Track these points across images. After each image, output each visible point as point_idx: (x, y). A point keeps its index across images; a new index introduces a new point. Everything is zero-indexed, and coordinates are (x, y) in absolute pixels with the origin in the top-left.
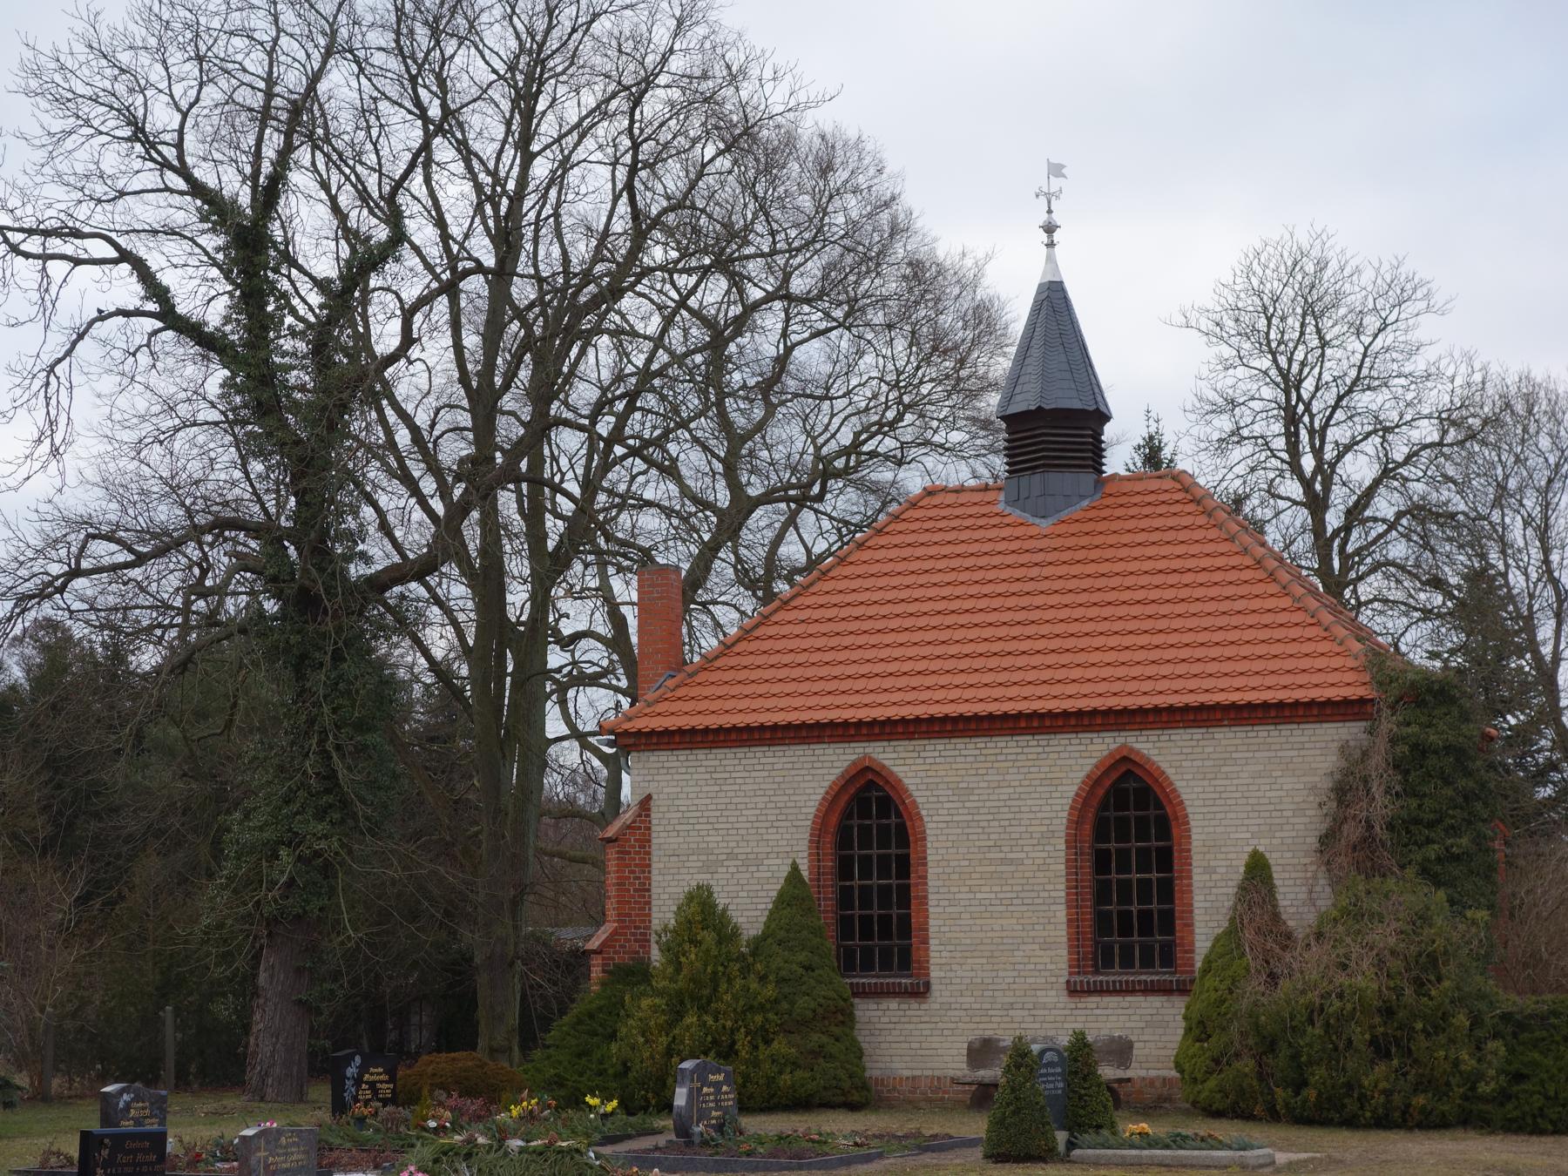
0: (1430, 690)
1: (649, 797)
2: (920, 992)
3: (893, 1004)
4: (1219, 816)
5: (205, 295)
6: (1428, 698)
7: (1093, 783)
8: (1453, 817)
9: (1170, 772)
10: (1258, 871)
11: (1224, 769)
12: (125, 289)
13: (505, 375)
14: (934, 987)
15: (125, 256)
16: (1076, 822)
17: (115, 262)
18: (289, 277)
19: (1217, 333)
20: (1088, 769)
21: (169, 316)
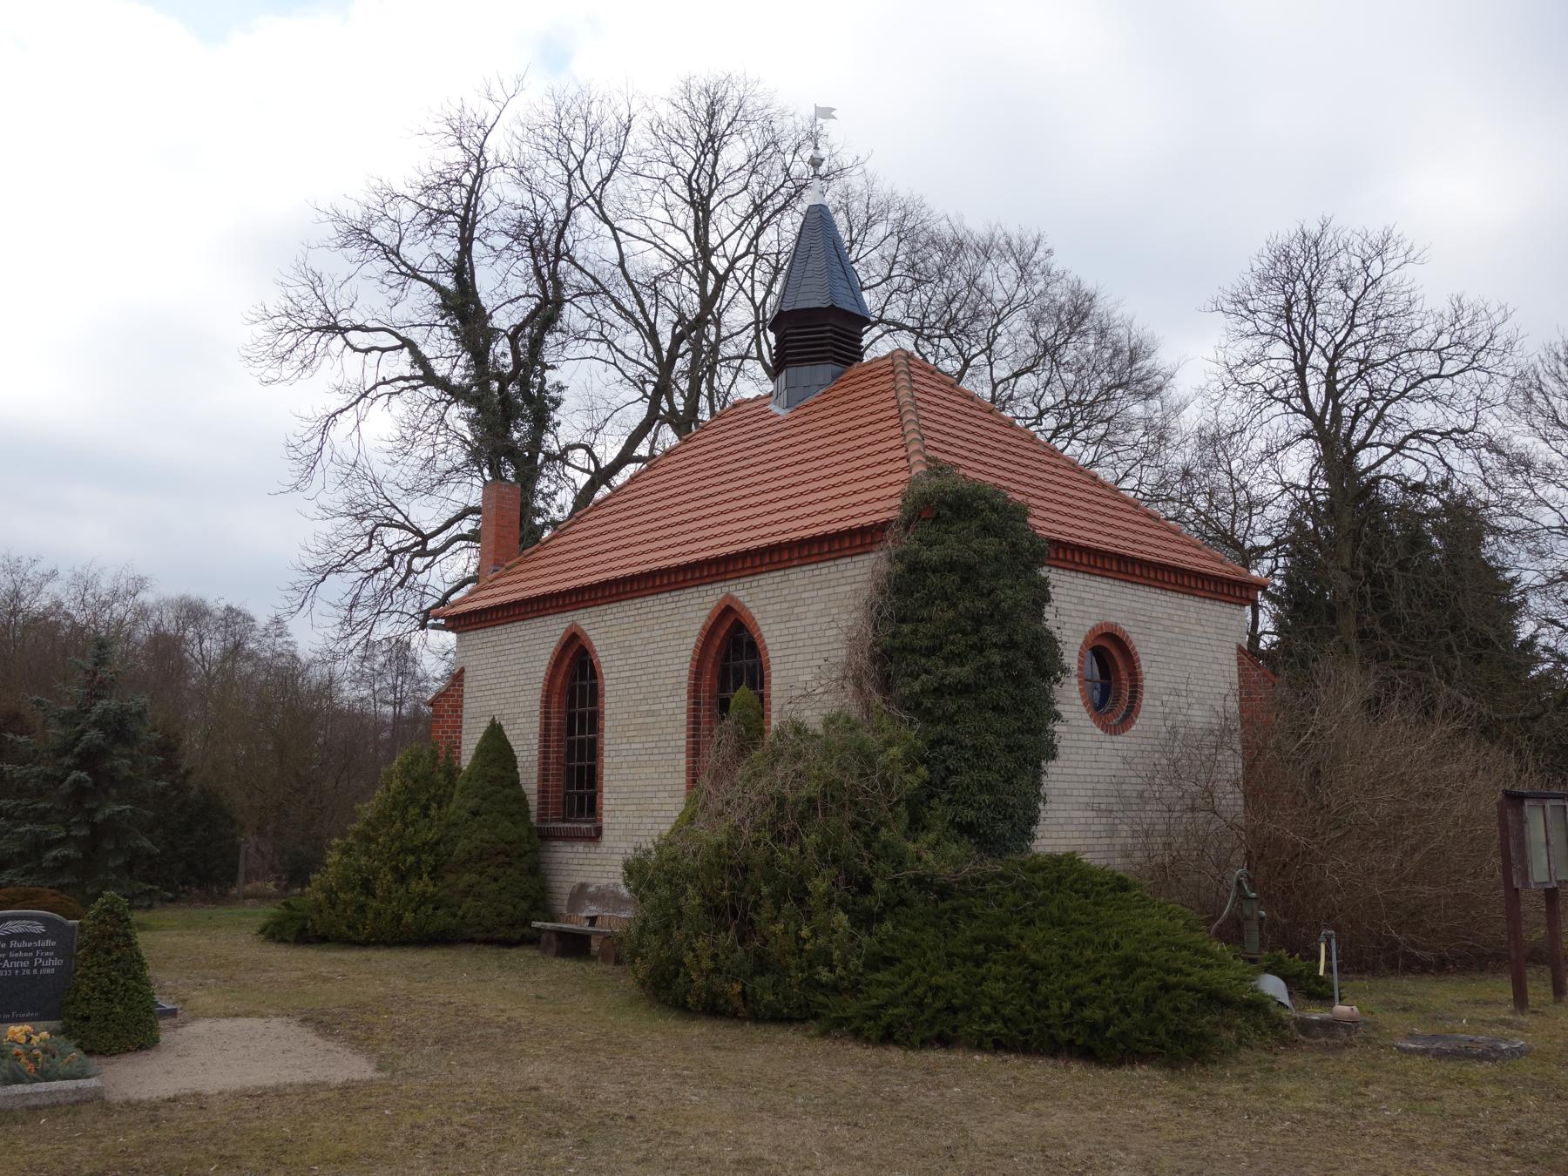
0: (942, 502)
1: (462, 671)
2: (595, 836)
3: (580, 847)
4: (792, 658)
5: (450, 361)
6: (945, 511)
7: (709, 633)
8: (953, 643)
9: (757, 617)
10: (495, 733)
11: (796, 610)
12: (401, 363)
13: (699, 393)
14: (605, 832)
15: (407, 343)
16: (697, 674)
17: (401, 347)
18: (1542, 502)
19: (1241, 305)
20: (704, 620)
21: (430, 378)
